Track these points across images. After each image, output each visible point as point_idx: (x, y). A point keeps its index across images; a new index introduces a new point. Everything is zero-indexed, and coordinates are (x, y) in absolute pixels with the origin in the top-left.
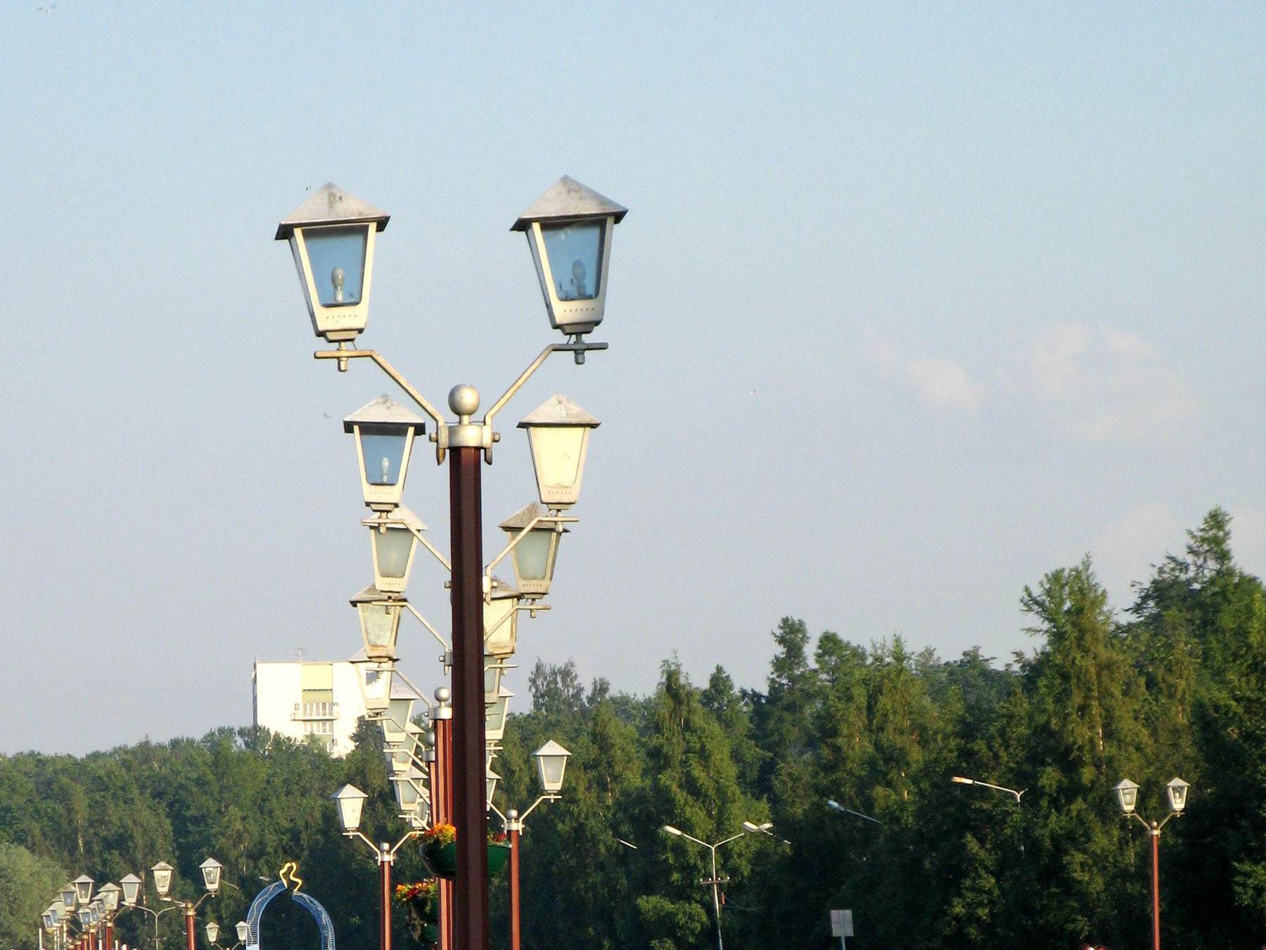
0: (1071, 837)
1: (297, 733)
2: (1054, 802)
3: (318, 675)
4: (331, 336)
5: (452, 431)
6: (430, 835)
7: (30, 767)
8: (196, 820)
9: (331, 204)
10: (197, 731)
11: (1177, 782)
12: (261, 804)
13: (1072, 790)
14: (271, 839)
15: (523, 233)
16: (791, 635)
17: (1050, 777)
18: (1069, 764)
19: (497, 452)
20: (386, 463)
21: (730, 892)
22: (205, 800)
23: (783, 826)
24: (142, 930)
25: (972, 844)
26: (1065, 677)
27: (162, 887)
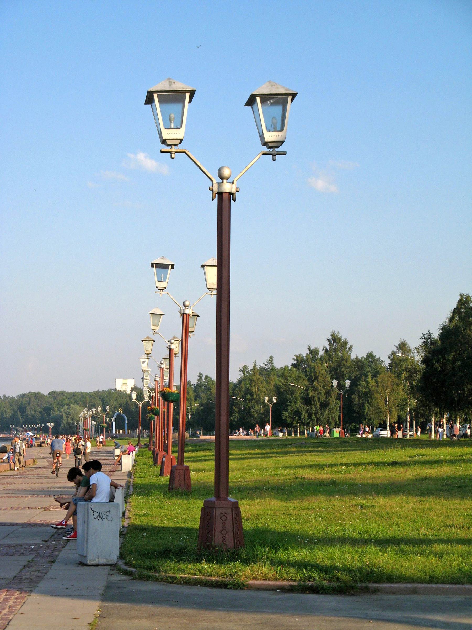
0: (252, 407)
1: (122, 390)
2: (249, 401)
3: (125, 381)
4: (168, 142)
5: (219, 185)
6: (163, 391)
7: (80, 394)
8: (106, 402)
9: (170, 85)
10: (106, 389)
11: (275, 397)
12: (116, 400)
13: (252, 399)
14: (117, 405)
15: (250, 107)
16: (200, 375)
17: (248, 397)
18: (251, 395)
19: (238, 195)
20: (163, 276)
21: (191, 415)
22: (107, 399)
23: (201, 404)
24: (97, 419)
25: (234, 408)
26: (251, 380)
27: (99, 411)
